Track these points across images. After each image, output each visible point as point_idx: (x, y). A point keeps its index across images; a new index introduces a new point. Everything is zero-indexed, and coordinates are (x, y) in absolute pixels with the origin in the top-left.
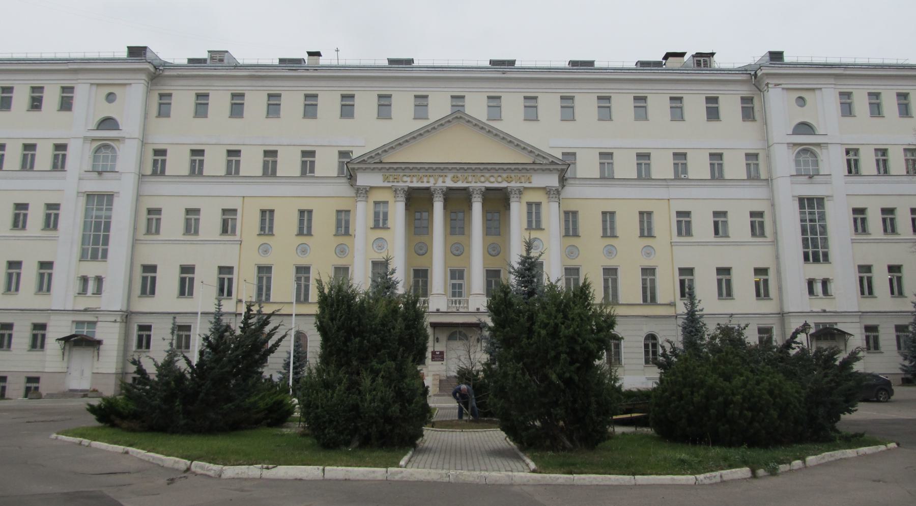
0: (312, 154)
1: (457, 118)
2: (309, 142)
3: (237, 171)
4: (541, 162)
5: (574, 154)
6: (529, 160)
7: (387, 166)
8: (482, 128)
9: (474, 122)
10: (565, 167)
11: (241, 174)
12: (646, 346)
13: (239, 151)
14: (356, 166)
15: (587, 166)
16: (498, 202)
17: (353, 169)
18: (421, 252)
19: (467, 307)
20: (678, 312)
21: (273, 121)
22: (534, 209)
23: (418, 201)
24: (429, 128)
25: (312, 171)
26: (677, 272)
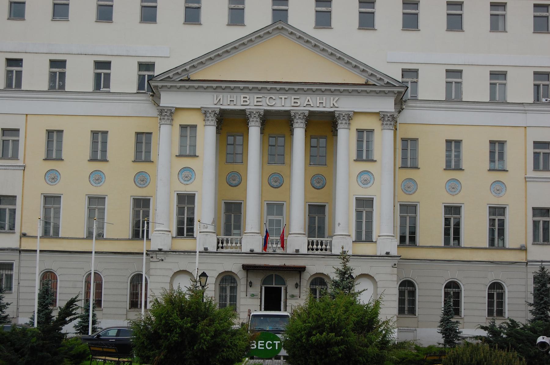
0: (107, 65)
1: (277, 28)
2: (104, 52)
3: (19, 84)
4: (372, 83)
5: (416, 71)
6: (361, 79)
7: (196, 85)
8: (307, 42)
9: (298, 34)
10: (403, 90)
11: (24, 87)
12: (490, 296)
13: (21, 60)
14: (160, 84)
15: (431, 86)
16: (324, 126)
17: (156, 87)
18: (234, 183)
19: (240, 247)
20: (530, 258)
21: (60, 25)
22: (364, 137)
23: (230, 124)
24: (245, 41)
25: (107, 85)
26: (530, 213)
